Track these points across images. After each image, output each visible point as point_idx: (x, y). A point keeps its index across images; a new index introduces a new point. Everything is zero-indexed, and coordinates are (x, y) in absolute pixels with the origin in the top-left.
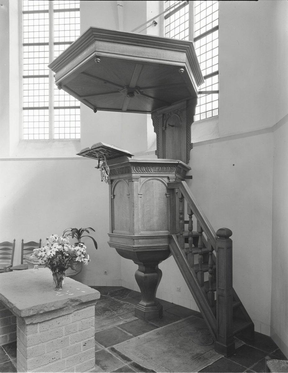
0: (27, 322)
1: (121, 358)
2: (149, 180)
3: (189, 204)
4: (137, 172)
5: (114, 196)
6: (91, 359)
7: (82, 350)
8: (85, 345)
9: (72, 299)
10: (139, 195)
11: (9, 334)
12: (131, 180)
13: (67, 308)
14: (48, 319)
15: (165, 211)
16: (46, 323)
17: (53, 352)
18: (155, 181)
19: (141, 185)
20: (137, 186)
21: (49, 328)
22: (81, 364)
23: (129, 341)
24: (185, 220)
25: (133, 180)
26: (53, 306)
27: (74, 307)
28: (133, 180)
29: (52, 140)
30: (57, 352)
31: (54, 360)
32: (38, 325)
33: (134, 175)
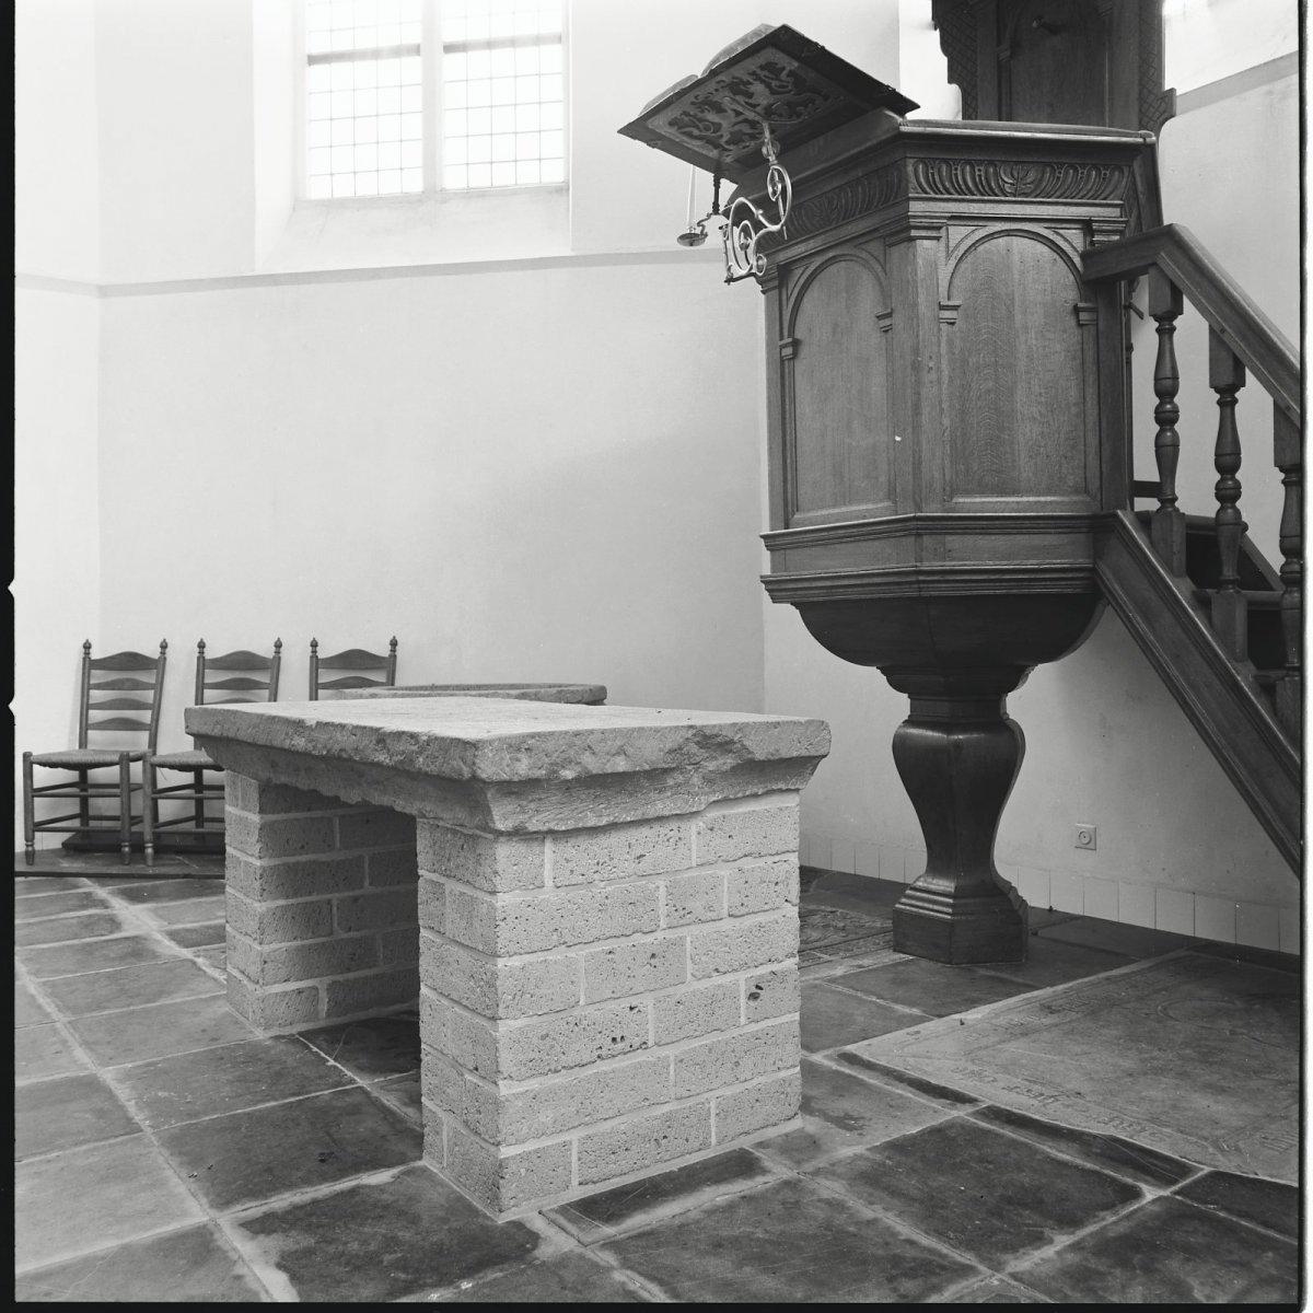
0: (503, 815)
1: (914, 1090)
2: (991, 236)
3: (1223, 331)
4: (933, 195)
5: (796, 344)
6: (783, 1074)
7: (743, 1020)
8: (754, 997)
9: (708, 732)
10: (942, 308)
11: (327, 980)
12: (900, 232)
13: (681, 779)
14: (592, 822)
15: (1073, 394)
16: (583, 842)
17: (612, 1005)
18: (1019, 244)
19: (953, 262)
20: (933, 266)
21: (596, 876)
22: (737, 1088)
23: (918, 1032)
24: (1137, 477)
25: (914, 233)
26: (621, 751)
27: (709, 780)
28: (914, 233)
29: (434, 195)
30: (631, 1009)
31: (620, 1046)
32: (549, 846)
33: (916, 207)
